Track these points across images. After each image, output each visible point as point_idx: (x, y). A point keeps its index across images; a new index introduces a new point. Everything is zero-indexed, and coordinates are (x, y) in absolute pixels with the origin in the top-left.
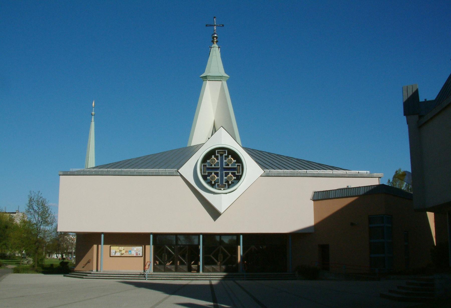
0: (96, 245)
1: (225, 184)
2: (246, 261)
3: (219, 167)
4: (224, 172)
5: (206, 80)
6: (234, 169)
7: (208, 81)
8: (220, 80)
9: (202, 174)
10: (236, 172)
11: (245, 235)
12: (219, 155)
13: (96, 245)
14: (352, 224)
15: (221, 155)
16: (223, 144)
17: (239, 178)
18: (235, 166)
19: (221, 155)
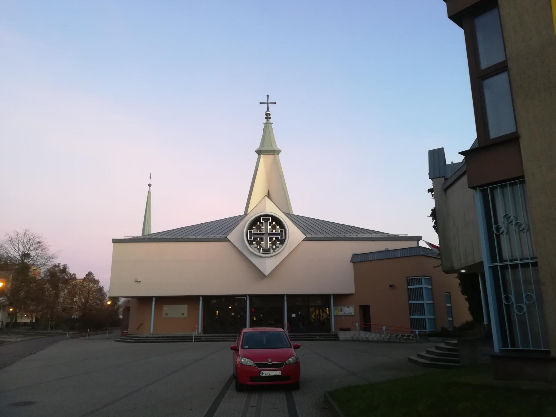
3: (264, 232)
6: (278, 234)
11: (291, 297)
12: (264, 222)
14: (390, 286)
15: (266, 222)
17: (282, 242)
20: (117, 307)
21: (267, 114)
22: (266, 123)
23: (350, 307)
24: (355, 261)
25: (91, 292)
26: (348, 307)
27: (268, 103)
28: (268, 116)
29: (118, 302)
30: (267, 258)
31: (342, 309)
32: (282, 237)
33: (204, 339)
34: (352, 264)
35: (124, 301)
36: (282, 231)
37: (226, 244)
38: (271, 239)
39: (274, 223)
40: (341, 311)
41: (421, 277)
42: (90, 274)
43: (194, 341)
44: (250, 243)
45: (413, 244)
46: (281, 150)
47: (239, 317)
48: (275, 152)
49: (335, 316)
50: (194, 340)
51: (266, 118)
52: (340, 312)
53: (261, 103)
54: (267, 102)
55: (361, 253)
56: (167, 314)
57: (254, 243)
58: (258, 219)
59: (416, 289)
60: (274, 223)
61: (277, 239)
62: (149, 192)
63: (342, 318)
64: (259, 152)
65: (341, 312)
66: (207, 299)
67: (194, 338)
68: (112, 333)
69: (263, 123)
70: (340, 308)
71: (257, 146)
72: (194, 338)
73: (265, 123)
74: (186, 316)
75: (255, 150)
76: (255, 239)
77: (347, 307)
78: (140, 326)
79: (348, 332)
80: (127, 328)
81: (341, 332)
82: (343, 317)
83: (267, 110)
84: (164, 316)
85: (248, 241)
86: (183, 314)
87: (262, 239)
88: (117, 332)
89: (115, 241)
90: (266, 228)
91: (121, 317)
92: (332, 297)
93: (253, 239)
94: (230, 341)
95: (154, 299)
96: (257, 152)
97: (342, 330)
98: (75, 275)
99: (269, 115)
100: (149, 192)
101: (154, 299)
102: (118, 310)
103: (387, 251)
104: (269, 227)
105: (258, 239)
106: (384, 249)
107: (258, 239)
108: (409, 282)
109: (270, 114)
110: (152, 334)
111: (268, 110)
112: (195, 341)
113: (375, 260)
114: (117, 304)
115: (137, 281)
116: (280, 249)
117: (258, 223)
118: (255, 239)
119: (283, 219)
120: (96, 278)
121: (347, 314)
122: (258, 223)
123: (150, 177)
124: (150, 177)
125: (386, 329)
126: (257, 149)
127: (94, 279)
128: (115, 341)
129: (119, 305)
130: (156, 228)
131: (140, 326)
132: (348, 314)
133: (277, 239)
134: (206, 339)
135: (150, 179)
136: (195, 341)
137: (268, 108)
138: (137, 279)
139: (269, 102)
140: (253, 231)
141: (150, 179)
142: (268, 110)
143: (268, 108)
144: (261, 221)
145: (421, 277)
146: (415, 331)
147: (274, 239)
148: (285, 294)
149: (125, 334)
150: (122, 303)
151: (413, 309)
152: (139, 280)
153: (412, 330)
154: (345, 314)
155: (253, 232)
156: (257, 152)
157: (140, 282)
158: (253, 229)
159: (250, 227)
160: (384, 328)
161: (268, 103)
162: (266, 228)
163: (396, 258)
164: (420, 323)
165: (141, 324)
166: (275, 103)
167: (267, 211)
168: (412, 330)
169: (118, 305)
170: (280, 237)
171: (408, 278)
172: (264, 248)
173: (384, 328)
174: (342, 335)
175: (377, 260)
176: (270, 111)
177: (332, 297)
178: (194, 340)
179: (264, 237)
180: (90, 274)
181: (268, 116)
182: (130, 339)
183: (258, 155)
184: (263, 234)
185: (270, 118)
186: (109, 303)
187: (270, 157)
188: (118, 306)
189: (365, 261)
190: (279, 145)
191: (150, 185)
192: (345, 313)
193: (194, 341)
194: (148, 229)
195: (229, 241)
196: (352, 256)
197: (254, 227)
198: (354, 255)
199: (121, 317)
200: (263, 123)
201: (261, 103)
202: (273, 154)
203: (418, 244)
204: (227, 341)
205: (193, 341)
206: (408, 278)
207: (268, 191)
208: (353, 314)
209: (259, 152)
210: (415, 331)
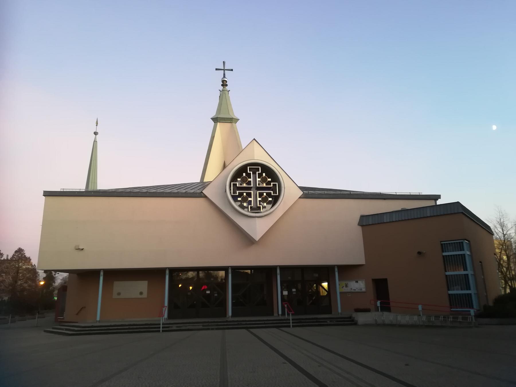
0: (295, 291)
1: (260, 206)
2: (190, 291)
3: (252, 186)
4: (258, 192)
5: (216, 122)
6: (269, 189)
7: (219, 122)
8: (230, 122)
9: (232, 194)
10: (272, 192)
11: (284, 269)
12: (251, 172)
13: (295, 291)
14: (419, 253)
15: (254, 173)
16: (256, 159)
17: (276, 199)
18: (271, 185)
19: (254, 173)
20: (52, 288)
21: (223, 81)
22: (223, 91)
23: (359, 282)
24: (364, 224)
25: (20, 271)
26: (357, 282)
27: (224, 70)
28: (224, 84)
29: (53, 284)
30: (257, 218)
31: (348, 284)
32: (275, 192)
33: (174, 327)
34: (360, 228)
35: (60, 283)
36: (275, 185)
37: (200, 201)
38: (261, 195)
39: (264, 174)
40: (346, 286)
41: (462, 241)
42: (20, 251)
43: (161, 331)
44: (235, 198)
45: (431, 203)
46: (239, 119)
47: (216, 296)
48: (232, 120)
49: (340, 293)
50: (161, 329)
51: (222, 85)
52: (344, 288)
53: (217, 69)
54: (223, 68)
55: (387, 212)
56: (119, 294)
57: (239, 199)
58: (243, 169)
59: (453, 256)
60: (264, 174)
61: (269, 195)
62: (95, 142)
63: (348, 296)
64: (216, 120)
65: (346, 288)
66: (174, 271)
67: (161, 326)
68: (44, 317)
69: (219, 90)
70: (346, 282)
71: (213, 114)
72: (161, 326)
73: (221, 90)
74: (145, 295)
75: (211, 117)
76: (241, 195)
77: (355, 282)
78: (81, 310)
79: (368, 314)
80: (62, 312)
81: (359, 314)
82: (350, 294)
83: (224, 77)
84: (115, 296)
85: (232, 196)
86: (141, 293)
87: (249, 195)
88: (50, 316)
89: (47, 194)
90: (254, 180)
91: (56, 298)
92: (336, 269)
93: (238, 194)
94: (213, 329)
95: (102, 273)
96: (212, 119)
97: (357, 310)
98: (4, 255)
99: (225, 82)
100: (95, 142)
101: (102, 273)
102: (54, 292)
103: (404, 211)
104: (258, 179)
105: (245, 194)
106: (400, 209)
107: (245, 194)
108: (444, 247)
109: (226, 81)
110: (99, 321)
111: (224, 77)
112: (163, 331)
113: (393, 222)
114: (52, 285)
115: (79, 249)
116: (267, 211)
117: (244, 174)
118: (241, 195)
119: (276, 168)
120: (27, 255)
121: (355, 290)
122: (244, 174)
123: (97, 124)
124: (97, 124)
125: (422, 309)
126: (212, 116)
127: (25, 256)
128: (45, 331)
129: (54, 287)
130: (102, 185)
131: (81, 310)
132: (357, 290)
133: (269, 195)
134: (177, 327)
135: (97, 126)
136: (163, 331)
137: (224, 74)
138: (79, 246)
139: (226, 68)
140: (237, 183)
141: (97, 126)
142: (224, 77)
143: (224, 74)
144: (248, 172)
145: (462, 241)
146: (470, 311)
147: (265, 194)
148: (277, 266)
149: (59, 320)
150: (57, 284)
151: (450, 282)
152: (81, 247)
153: (452, 309)
154: (352, 290)
155: (238, 186)
156: (212, 119)
157: (82, 249)
158: (237, 181)
159: (234, 179)
160: (420, 307)
161: (224, 70)
162: (254, 180)
163: (455, 213)
164: (466, 301)
165: (82, 308)
166: (232, 70)
167: (255, 159)
168: (452, 309)
169: (53, 286)
170: (272, 192)
171: (442, 243)
172: (252, 206)
173: (420, 307)
174: (362, 318)
175: (396, 221)
176: (226, 78)
177: (336, 269)
178: (161, 329)
179: (252, 192)
180: (20, 251)
181: (224, 84)
182: (66, 330)
183: (214, 122)
184: (250, 189)
185: (227, 85)
186: (42, 283)
187: (227, 125)
188: (53, 287)
189: (378, 224)
190: (236, 113)
191: (96, 133)
192: (351, 289)
193: (161, 331)
194: (93, 182)
195: (205, 197)
196: (359, 217)
197: (239, 179)
198: (362, 217)
199: (56, 298)
200: (219, 90)
201: (217, 69)
202: (231, 123)
203: (436, 203)
204: (208, 329)
205: (159, 331)
206: (442, 243)
207: (224, 162)
208: (364, 290)
209: (216, 120)
210: (470, 311)
